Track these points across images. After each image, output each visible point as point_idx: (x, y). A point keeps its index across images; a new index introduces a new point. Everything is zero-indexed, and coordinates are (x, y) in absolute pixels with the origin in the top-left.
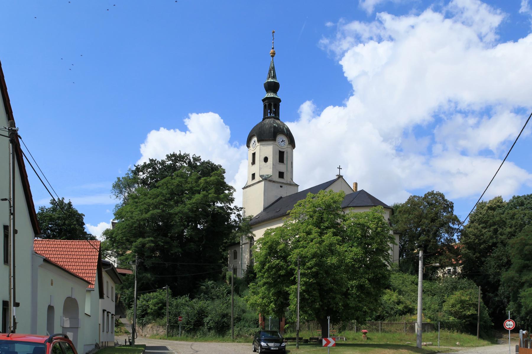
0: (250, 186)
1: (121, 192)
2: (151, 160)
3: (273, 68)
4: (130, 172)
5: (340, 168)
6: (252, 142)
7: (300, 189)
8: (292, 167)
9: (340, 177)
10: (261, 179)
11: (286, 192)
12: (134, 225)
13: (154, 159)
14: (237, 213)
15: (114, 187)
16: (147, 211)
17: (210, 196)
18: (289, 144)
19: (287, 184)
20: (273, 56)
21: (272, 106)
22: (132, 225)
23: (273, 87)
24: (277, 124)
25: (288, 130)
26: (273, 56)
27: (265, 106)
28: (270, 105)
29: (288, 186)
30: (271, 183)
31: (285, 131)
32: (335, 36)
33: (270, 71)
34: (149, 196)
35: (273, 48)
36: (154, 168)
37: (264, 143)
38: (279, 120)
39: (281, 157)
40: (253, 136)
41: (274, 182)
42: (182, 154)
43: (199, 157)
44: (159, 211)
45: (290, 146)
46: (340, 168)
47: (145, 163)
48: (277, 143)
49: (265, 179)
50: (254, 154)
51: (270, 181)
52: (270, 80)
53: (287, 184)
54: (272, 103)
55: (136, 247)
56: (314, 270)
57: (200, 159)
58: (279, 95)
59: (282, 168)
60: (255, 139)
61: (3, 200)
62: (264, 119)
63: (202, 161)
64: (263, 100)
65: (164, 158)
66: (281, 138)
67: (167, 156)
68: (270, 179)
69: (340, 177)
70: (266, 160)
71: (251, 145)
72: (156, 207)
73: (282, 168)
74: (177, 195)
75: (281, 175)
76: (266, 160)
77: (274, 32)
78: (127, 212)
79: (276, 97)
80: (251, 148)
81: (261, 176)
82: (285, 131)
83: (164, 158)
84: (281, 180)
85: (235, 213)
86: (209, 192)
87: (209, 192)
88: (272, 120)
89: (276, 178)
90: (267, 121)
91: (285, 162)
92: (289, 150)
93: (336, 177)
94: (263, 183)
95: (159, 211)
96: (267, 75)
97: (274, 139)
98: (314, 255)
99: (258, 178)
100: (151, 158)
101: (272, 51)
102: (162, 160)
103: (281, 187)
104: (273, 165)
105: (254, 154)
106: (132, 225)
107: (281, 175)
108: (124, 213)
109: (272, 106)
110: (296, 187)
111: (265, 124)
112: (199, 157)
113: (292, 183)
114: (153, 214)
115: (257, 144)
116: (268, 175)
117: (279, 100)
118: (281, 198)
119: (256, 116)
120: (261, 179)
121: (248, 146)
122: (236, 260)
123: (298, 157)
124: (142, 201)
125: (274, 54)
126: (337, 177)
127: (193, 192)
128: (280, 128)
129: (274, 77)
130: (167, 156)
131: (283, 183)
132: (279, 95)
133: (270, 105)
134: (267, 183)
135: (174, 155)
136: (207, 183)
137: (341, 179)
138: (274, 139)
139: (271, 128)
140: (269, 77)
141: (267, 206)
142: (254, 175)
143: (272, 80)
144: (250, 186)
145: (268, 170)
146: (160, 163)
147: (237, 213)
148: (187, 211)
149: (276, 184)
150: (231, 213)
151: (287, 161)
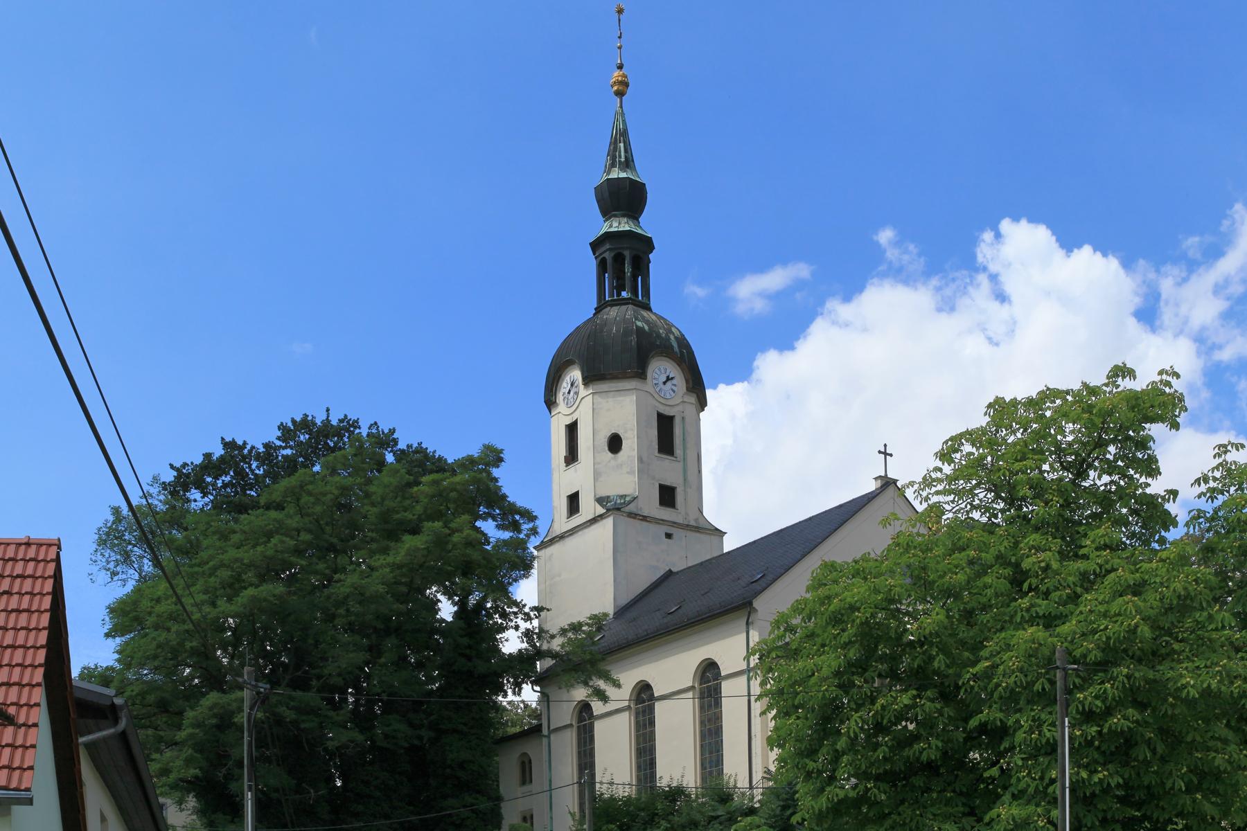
0: (562, 537)
1: (127, 558)
2: (229, 445)
3: (623, 134)
4: (154, 490)
5: (885, 454)
6: (565, 385)
7: (729, 544)
8: (700, 471)
9: (887, 483)
10: (600, 510)
11: (683, 555)
12: (188, 645)
13: (240, 443)
14: (524, 625)
15: (102, 542)
16: (234, 586)
17: (456, 538)
18: (688, 389)
19: (687, 527)
20: (620, 94)
22: (181, 644)
23: (624, 197)
24: (647, 322)
25: (683, 343)
26: (620, 94)
27: (602, 266)
28: (619, 259)
29: (689, 534)
30: (637, 523)
31: (675, 345)
33: (614, 144)
34: (235, 538)
35: (620, 67)
36: (240, 474)
37: (604, 386)
38: (649, 309)
39: (668, 435)
41: (645, 518)
42: (334, 422)
43: (392, 431)
44: (280, 589)
45: (692, 399)
46: (885, 454)
47: (208, 456)
48: (648, 386)
49: (613, 507)
50: (572, 429)
51: (632, 515)
52: (616, 174)
53: (687, 527)
54: (627, 253)
55: (198, 725)
56: (1115, 721)
57: (396, 442)
58: (648, 224)
59: (668, 471)
60: (575, 374)
62: (598, 310)
63: (402, 445)
64: (595, 246)
65: (273, 435)
66: (660, 368)
67: (282, 427)
68: (631, 508)
69: (887, 483)
70: (615, 443)
71: (560, 398)
72: (268, 571)
73: (668, 471)
74: (336, 535)
75: (667, 496)
76: (615, 443)
77: (620, 11)
78: (158, 600)
79: (640, 231)
81: (600, 501)
82: (675, 345)
83: (273, 435)
84: (666, 514)
85: (517, 628)
86: (453, 525)
87: (453, 525)
88: (629, 311)
89: (651, 505)
90: (612, 313)
91: (678, 451)
92: (690, 410)
93: (871, 486)
94: (609, 523)
95: (280, 589)
96: (603, 158)
97: (641, 374)
99: (588, 508)
100: (228, 439)
101: (617, 74)
102: (267, 446)
103: (669, 536)
104: (640, 460)
105: (572, 429)
106: (181, 644)
107: (667, 496)
108: (145, 604)
110: (714, 539)
111: (605, 323)
112: (392, 431)
113: (702, 524)
114: (254, 599)
115: (583, 392)
116: (622, 497)
117: (646, 244)
118: (669, 574)
119: (575, 298)
120: (600, 510)
121: (550, 403)
124: (211, 558)
125: (626, 85)
126: (879, 483)
127: (393, 531)
128: (659, 335)
129: (628, 164)
130: (282, 427)
131: (674, 524)
132: (648, 224)
133: (619, 259)
134: (624, 520)
135: (305, 424)
136: (441, 495)
137: (892, 488)
138: (641, 374)
139: (627, 333)
140: (613, 165)
141: (624, 601)
143: (623, 175)
144: (562, 537)
145: (625, 477)
146: (258, 457)
147: (524, 625)
148: (381, 589)
149: (653, 528)
150: (502, 629)
151: (685, 449)
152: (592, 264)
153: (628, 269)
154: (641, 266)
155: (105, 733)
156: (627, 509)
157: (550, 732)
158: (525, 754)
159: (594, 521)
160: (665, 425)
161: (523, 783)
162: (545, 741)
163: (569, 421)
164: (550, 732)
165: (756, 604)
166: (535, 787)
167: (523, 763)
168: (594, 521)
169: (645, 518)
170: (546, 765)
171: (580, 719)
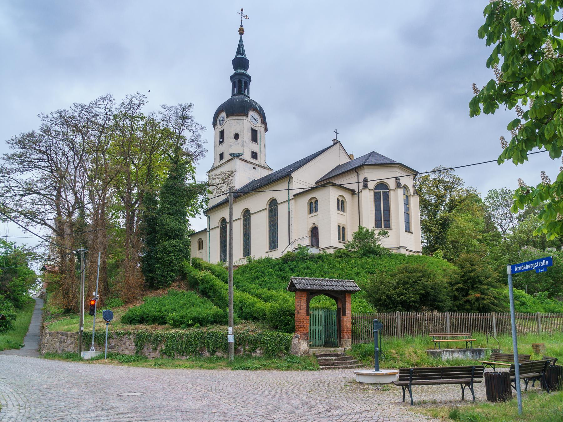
0: (217, 168)
5: (336, 132)
6: (220, 118)
10: (231, 157)
19: (260, 166)
21: (241, 82)
23: (241, 62)
25: (260, 107)
27: (234, 86)
32: (191, 186)
40: (222, 111)
41: (246, 161)
46: (336, 133)
50: (222, 133)
52: (239, 56)
53: (260, 166)
58: (249, 72)
59: (255, 147)
60: (224, 114)
61: (241, 62)
64: (231, 77)
66: (251, 113)
70: (237, 136)
73: (255, 147)
75: (254, 155)
77: (242, 10)
80: (218, 126)
81: (231, 155)
84: (253, 161)
89: (248, 156)
91: (258, 142)
97: (247, 115)
98: (34, 221)
99: (227, 157)
103: (254, 168)
105: (222, 133)
107: (254, 155)
109: (241, 82)
119: (225, 92)
120: (231, 157)
122: (201, 251)
123: (267, 138)
131: (256, 165)
133: (240, 82)
142: (222, 156)
144: (217, 168)
149: (249, 165)
151: (260, 141)
152: (230, 84)
153: (243, 85)
154: (247, 86)
155: (99, 257)
156: (240, 157)
157: (210, 230)
158: (200, 239)
159: (229, 161)
160: (254, 133)
161: (199, 249)
162: (208, 233)
163: (221, 130)
164: (210, 230)
165: (293, 175)
166: (203, 250)
167: (200, 242)
168: (229, 161)
169: (246, 161)
170: (208, 242)
171: (222, 225)
